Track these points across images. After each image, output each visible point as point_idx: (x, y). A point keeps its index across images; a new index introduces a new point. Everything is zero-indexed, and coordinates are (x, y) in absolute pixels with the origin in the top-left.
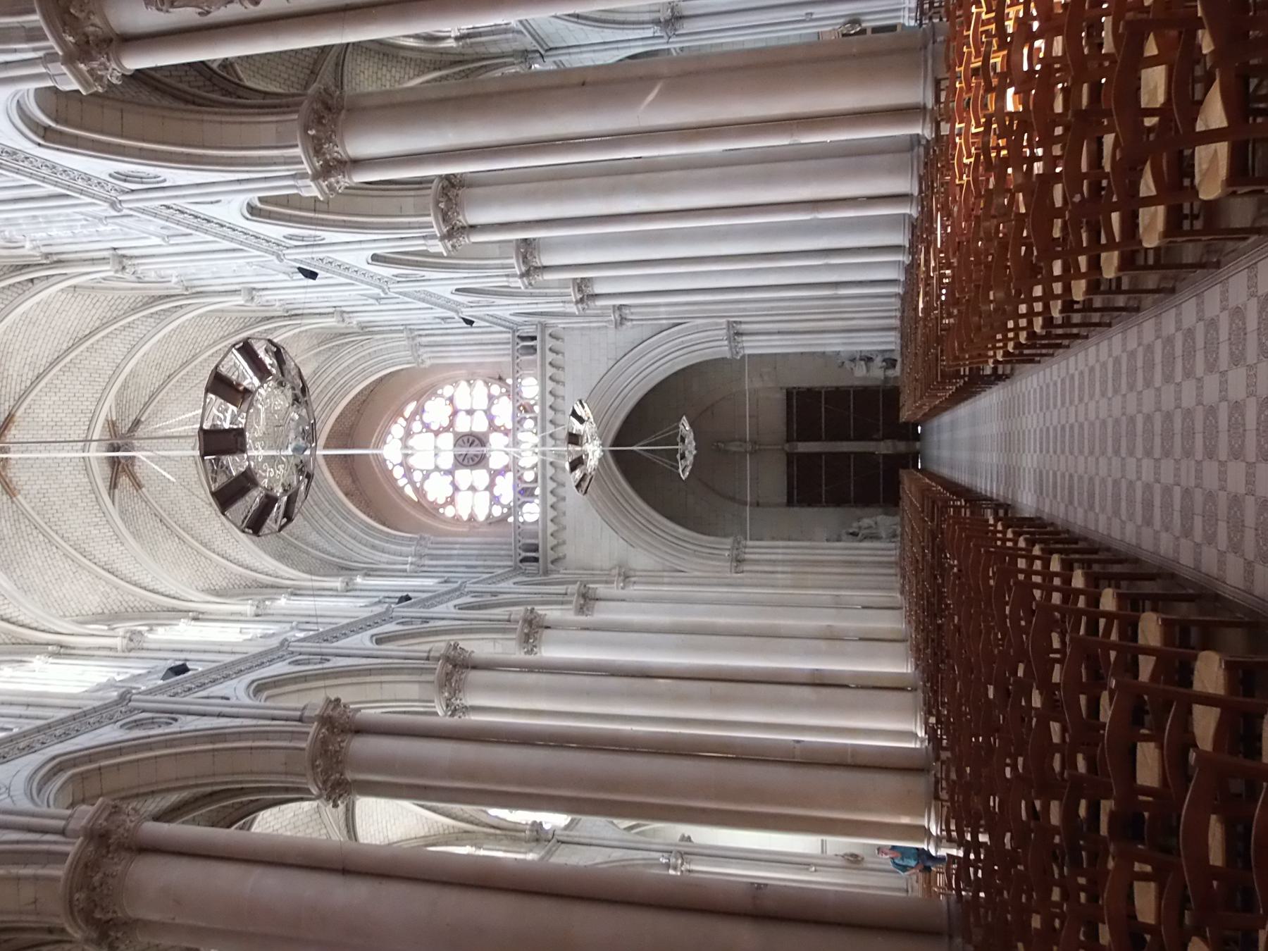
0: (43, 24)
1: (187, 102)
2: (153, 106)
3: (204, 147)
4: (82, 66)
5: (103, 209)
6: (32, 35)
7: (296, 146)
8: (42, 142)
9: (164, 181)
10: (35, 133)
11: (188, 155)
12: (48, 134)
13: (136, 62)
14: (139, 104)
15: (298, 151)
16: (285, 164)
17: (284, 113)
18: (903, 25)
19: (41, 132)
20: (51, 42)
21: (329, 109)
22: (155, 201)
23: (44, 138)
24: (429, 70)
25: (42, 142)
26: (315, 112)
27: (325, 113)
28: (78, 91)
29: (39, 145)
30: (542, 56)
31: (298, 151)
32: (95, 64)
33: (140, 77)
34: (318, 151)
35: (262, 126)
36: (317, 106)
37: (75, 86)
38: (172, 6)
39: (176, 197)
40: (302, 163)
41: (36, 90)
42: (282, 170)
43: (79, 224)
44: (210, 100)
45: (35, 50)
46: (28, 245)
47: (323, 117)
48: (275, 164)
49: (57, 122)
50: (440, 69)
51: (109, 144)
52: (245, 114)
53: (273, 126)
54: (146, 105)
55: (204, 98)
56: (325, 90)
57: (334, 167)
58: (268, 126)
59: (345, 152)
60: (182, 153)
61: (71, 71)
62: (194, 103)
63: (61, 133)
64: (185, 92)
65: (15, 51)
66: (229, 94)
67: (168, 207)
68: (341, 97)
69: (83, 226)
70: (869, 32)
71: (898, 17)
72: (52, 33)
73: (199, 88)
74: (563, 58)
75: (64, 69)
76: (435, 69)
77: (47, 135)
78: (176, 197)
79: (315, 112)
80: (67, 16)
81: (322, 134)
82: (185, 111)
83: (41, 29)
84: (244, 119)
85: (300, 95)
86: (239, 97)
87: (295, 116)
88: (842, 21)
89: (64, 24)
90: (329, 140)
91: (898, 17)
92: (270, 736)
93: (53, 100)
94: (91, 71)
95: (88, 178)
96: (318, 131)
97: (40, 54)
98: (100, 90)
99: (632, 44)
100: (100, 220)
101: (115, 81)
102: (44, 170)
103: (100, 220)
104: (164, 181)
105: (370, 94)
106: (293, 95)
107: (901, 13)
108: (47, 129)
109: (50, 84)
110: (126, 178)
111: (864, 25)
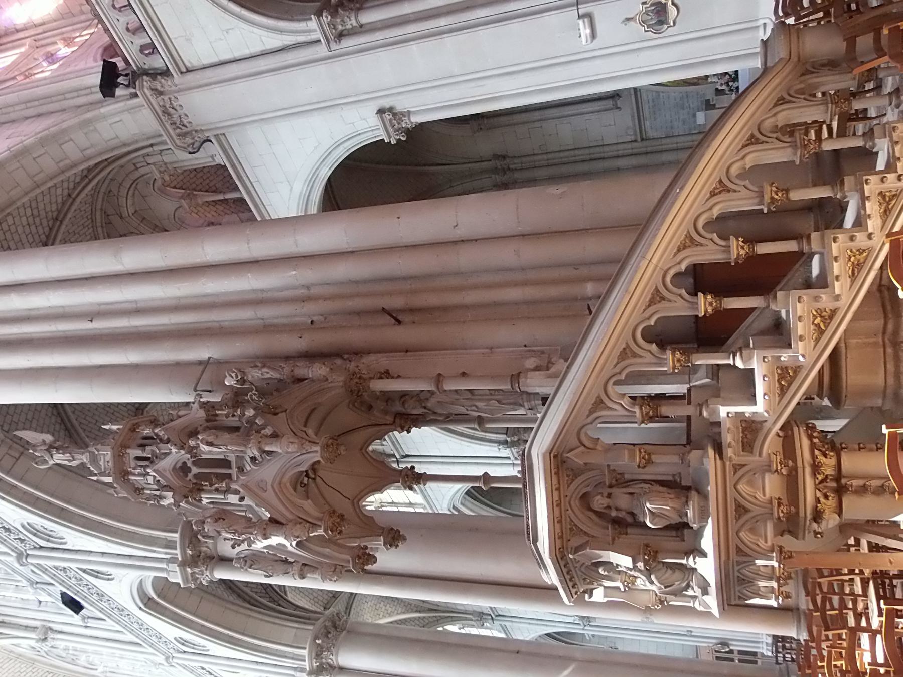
0: (178, 540)
1: (245, 600)
2: (224, 600)
3: (243, 634)
4: (189, 570)
5: (161, 659)
6: (169, 545)
7: (305, 648)
8: (143, 607)
9: (208, 650)
10: (142, 601)
11: (231, 637)
12: (150, 603)
13: (221, 574)
14: (214, 595)
15: (305, 653)
16: (293, 659)
17: (304, 623)
18: (762, 654)
19: (146, 601)
20: (178, 551)
21: (335, 627)
22: (196, 662)
23: (145, 605)
24: (412, 612)
25: (143, 607)
26: (326, 627)
27: (332, 630)
28: (178, 584)
29: (141, 609)
30: (492, 619)
31: (305, 653)
32: (196, 570)
33: (222, 581)
34: (318, 656)
35: (287, 629)
36: (328, 624)
37: (179, 580)
38: (250, 567)
39: (211, 663)
40: (304, 661)
41: (155, 577)
42: (289, 663)
43: (140, 664)
44: (261, 603)
45: (166, 553)
46: (101, 669)
47: (330, 633)
48: (286, 657)
49: (159, 596)
50: (420, 612)
51: (184, 618)
52: (278, 618)
53: (295, 630)
54: (220, 598)
55: (257, 601)
56: (337, 614)
57: (326, 670)
58: (290, 630)
59: (337, 660)
60: (228, 635)
61: (181, 570)
62: (249, 603)
63: (158, 603)
64: (247, 594)
65: (154, 551)
66: (273, 601)
67: (203, 669)
68: (346, 622)
69: (143, 666)
70: (736, 653)
71: (758, 648)
72: (181, 548)
73: (256, 593)
74: (507, 624)
75: (177, 569)
76: (416, 611)
77: (148, 603)
78: (211, 663)
79: (326, 627)
80: (193, 539)
81: (324, 644)
82: (242, 607)
83: (176, 542)
84: (277, 621)
85: (319, 613)
86: (279, 605)
87: (311, 628)
88: (714, 641)
89: (190, 542)
90: (328, 650)
91: (758, 648)
92: (291, 656)
93: (164, 587)
94: (193, 574)
95: (160, 637)
96: (323, 642)
97: (168, 556)
98: (193, 586)
99: (557, 624)
100: (155, 664)
101: (204, 583)
102: (136, 625)
103: (155, 664)
104: (208, 650)
105: (368, 624)
106: (315, 612)
107: (760, 645)
108: (150, 599)
109: (164, 575)
110: (184, 642)
111: (732, 648)
